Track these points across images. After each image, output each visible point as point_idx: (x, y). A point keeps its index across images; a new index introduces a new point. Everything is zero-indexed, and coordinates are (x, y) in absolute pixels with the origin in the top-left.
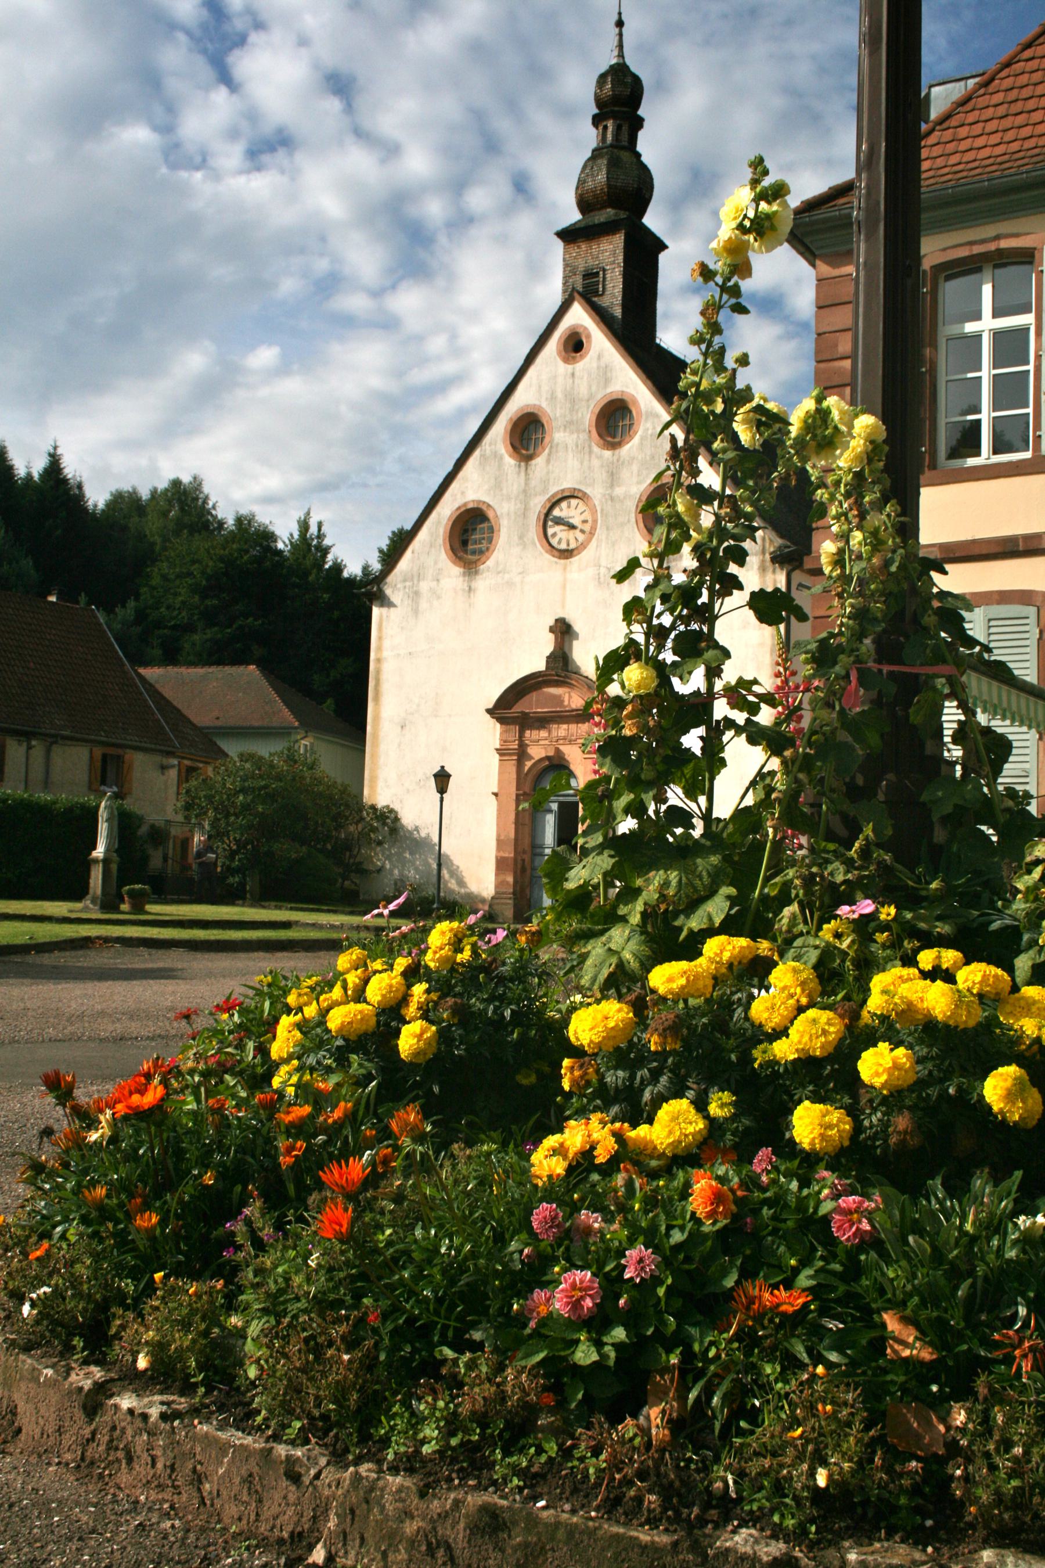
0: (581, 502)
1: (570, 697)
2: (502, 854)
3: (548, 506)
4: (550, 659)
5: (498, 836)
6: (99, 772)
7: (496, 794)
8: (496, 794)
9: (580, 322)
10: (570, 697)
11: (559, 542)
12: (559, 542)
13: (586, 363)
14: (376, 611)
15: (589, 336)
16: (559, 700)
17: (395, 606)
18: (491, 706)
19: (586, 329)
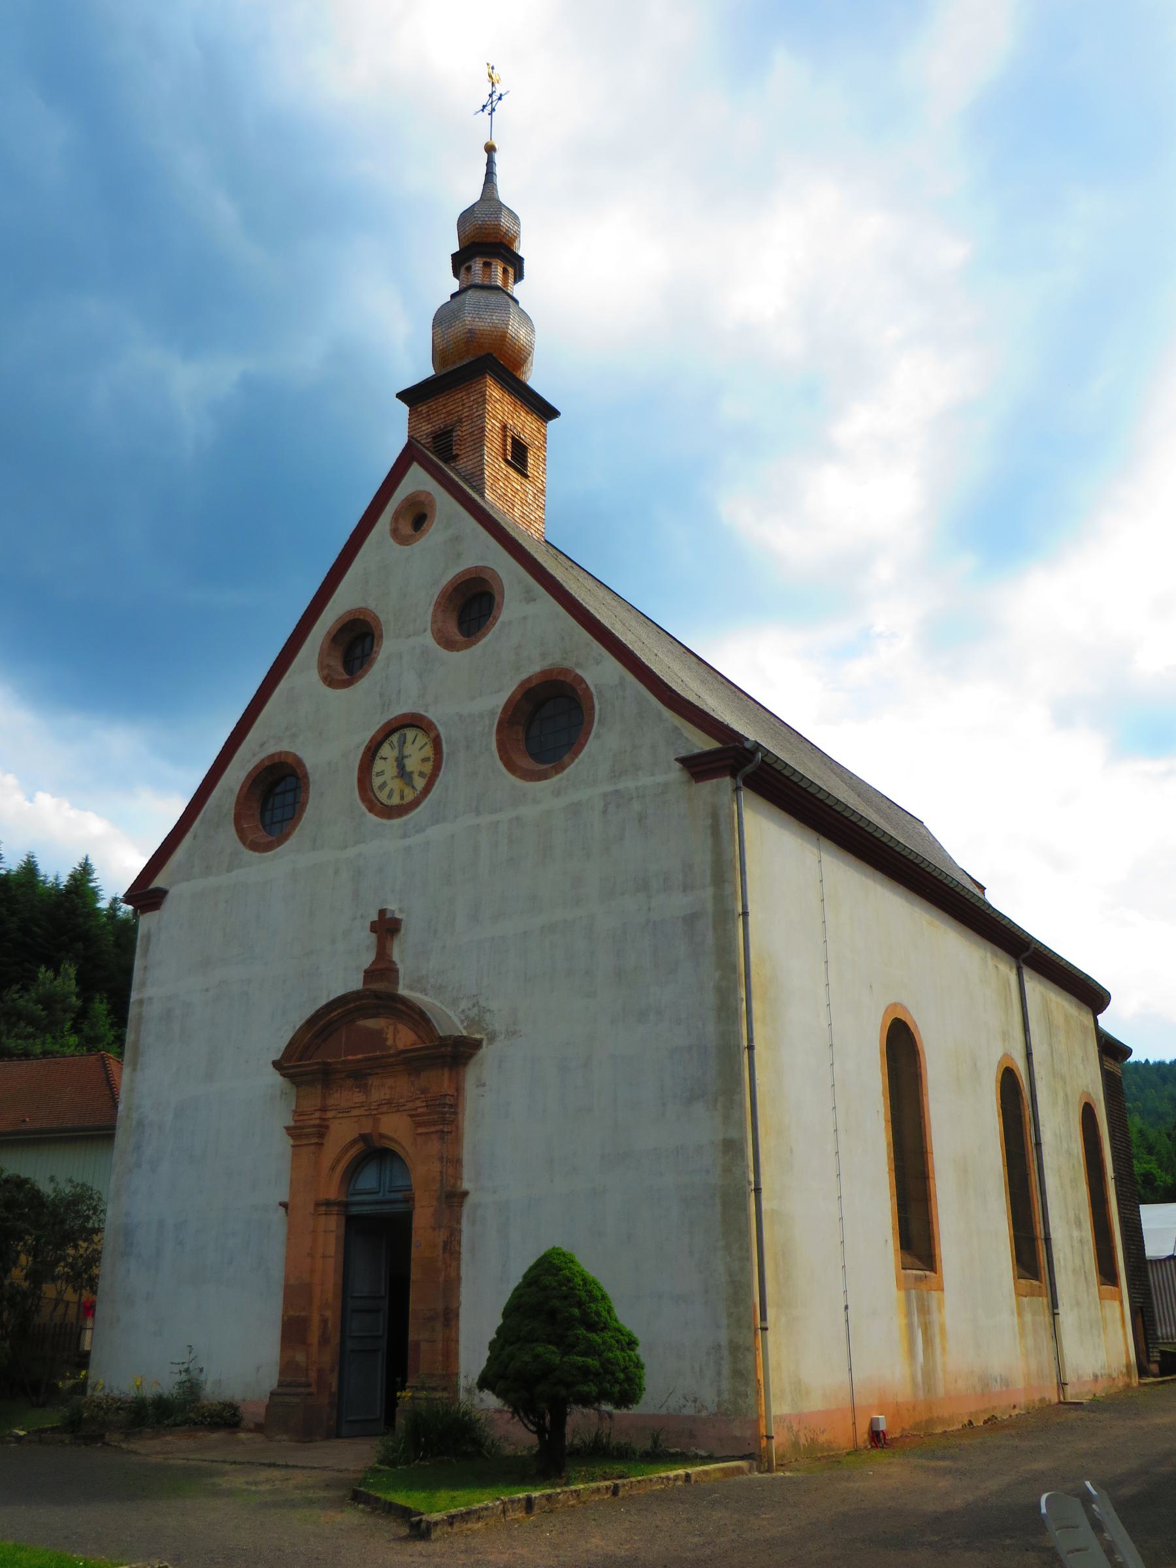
0: (420, 734)
1: (396, 1032)
2: (291, 1313)
3: (409, 722)
4: (369, 975)
5: (287, 1279)
6: (627, 638)
7: (284, 1205)
8: (284, 1205)
9: (421, 488)
10: (396, 1032)
11: (390, 796)
12: (390, 796)
13: (435, 535)
14: (727, 781)
15: (432, 504)
16: (377, 1037)
17: (676, 760)
18: (277, 1057)
19: (429, 494)
